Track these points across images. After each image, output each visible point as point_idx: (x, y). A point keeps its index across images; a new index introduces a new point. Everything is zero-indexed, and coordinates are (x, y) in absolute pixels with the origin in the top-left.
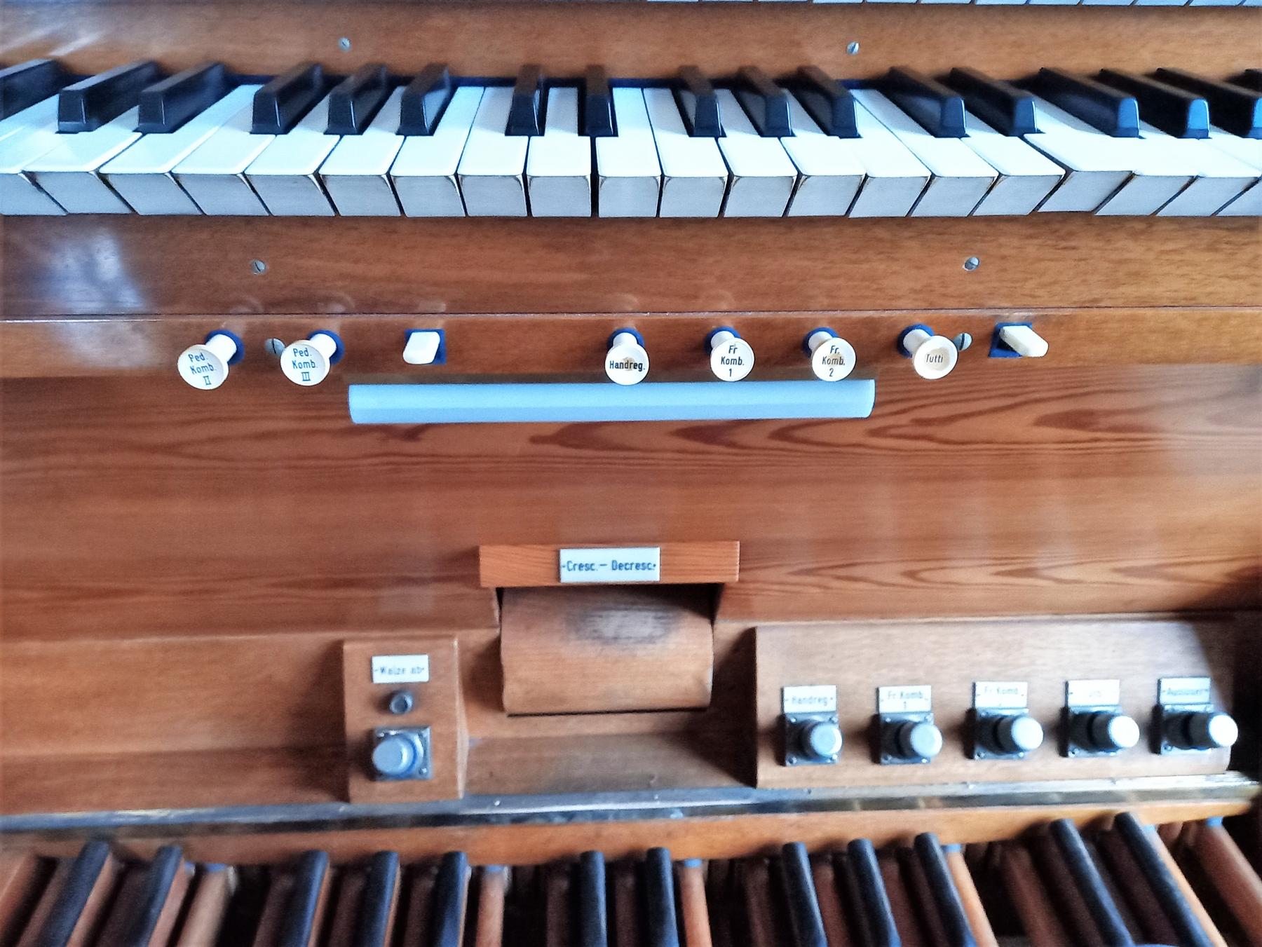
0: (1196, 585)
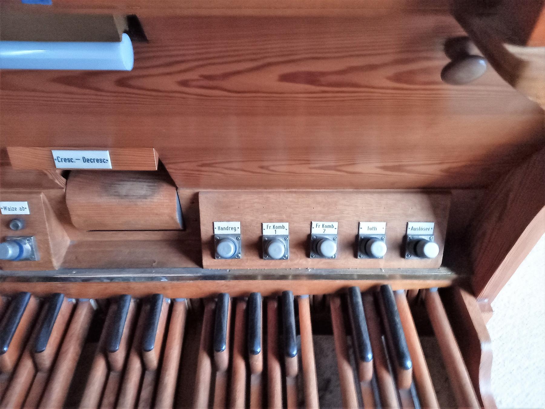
0: (427, 176)
